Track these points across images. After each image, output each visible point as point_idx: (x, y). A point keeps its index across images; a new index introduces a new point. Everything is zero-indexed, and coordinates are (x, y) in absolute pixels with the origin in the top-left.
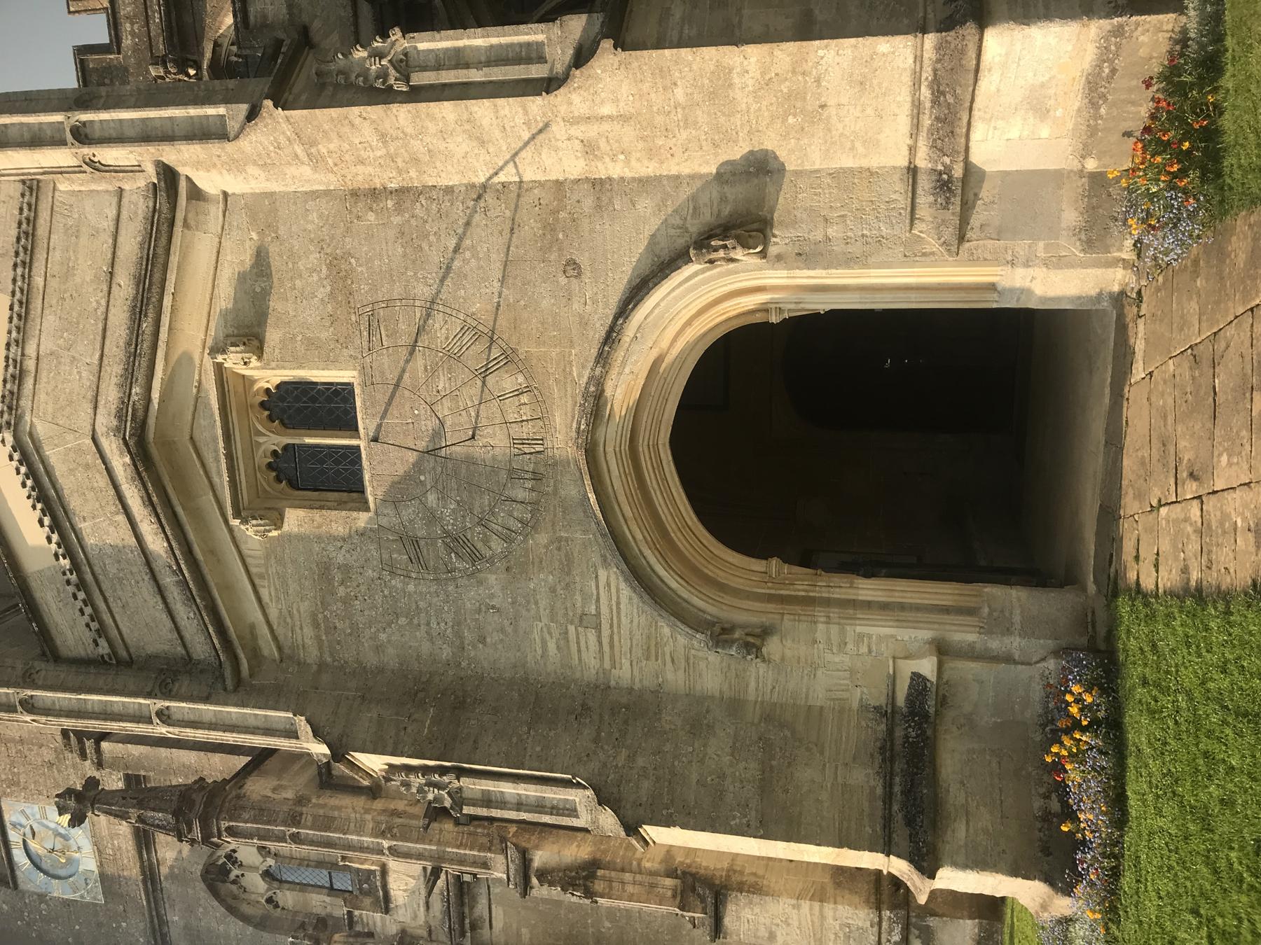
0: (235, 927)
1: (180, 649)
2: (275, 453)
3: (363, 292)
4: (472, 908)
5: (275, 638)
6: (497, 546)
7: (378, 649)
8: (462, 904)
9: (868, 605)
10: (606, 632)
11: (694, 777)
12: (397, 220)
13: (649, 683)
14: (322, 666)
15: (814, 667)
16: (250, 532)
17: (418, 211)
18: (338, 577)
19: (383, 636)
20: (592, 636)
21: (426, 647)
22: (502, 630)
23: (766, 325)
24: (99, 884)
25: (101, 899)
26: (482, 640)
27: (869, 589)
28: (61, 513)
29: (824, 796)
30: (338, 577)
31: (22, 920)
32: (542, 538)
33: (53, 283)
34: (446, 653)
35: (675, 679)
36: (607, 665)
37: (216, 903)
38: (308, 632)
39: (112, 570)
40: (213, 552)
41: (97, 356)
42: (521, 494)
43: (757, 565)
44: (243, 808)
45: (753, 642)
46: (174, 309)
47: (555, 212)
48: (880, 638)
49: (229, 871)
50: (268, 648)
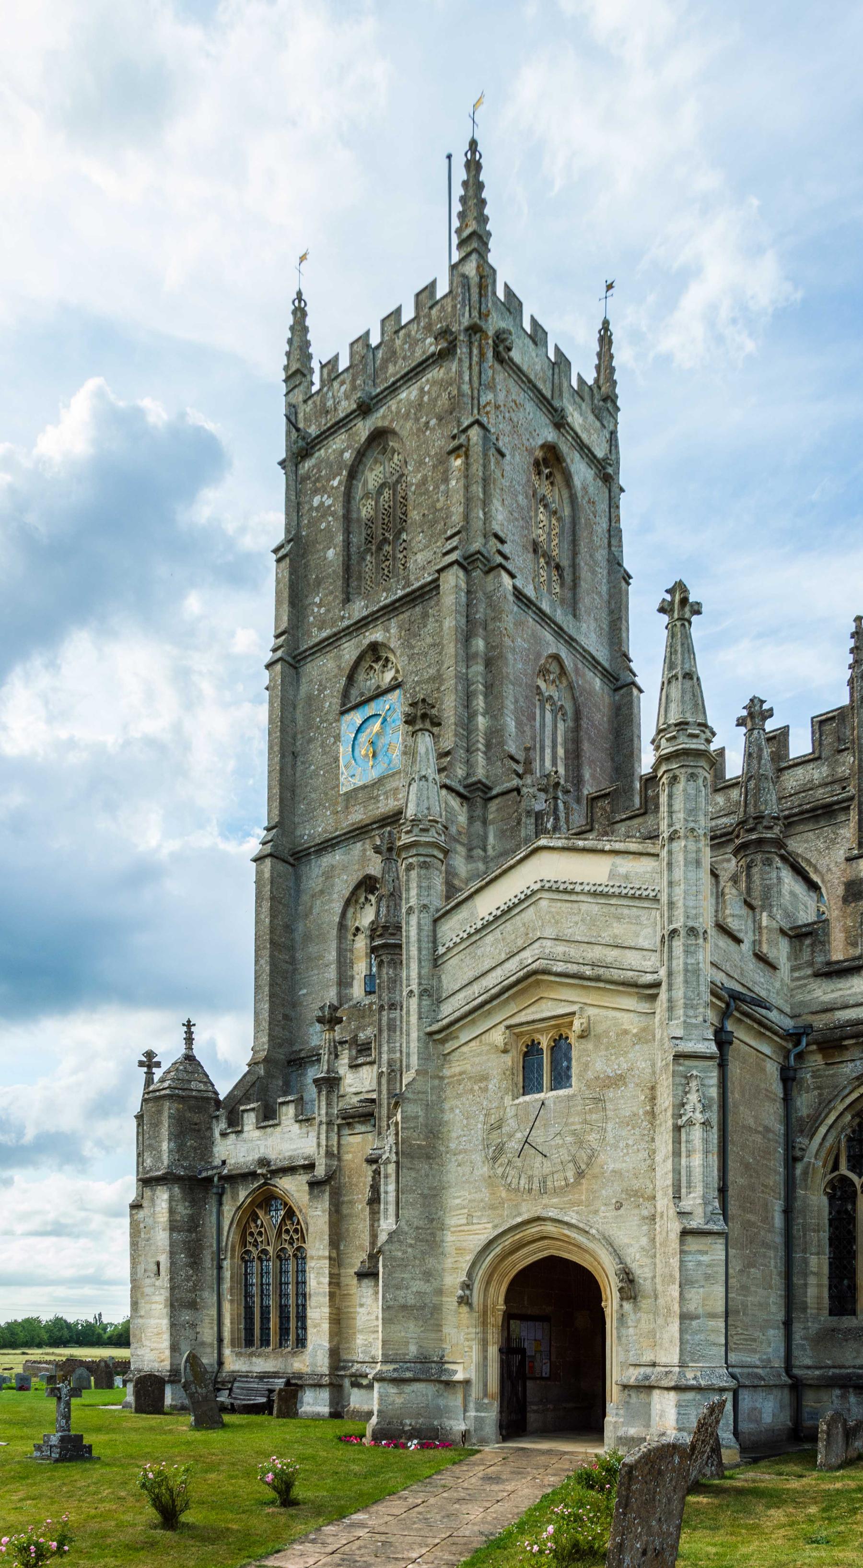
0: (337, 907)
1: (444, 995)
2: (539, 1043)
3: (610, 1094)
4: (359, 1122)
5: (453, 1051)
6: (500, 1171)
7: (452, 1109)
8: (360, 1117)
9: (485, 1350)
10: (466, 1228)
11: (405, 1276)
12: (641, 1112)
13: (447, 1250)
14: (442, 1078)
15: (458, 1327)
16: (498, 1037)
17: (645, 1123)
18: (482, 1085)
19: (457, 1111)
20: (464, 1221)
21: (454, 1135)
22: (464, 1175)
23: (601, 1300)
24: (352, 787)
25: (343, 790)
26: (459, 1165)
27: (493, 1351)
28: (503, 919)
29: (403, 1334)
30: (482, 1085)
31: (321, 722)
32: (504, 1194)
33: (613, 909)
34: (453, 1146)
35: (449, 1262)
36: (452, 1229)
37: (351, 889)
38: (457, 1070)
39: (479, 952)
40: (489, 1012)
41: (579, 939)
42: (522, 1182)
43: (501, 1300)
44: (395, 968)
45: (464, 1301)
46: (599, 988)
47: (642, 1196)
48: (471, 1357)
49: (373, 894)
50: (449, 1046)
